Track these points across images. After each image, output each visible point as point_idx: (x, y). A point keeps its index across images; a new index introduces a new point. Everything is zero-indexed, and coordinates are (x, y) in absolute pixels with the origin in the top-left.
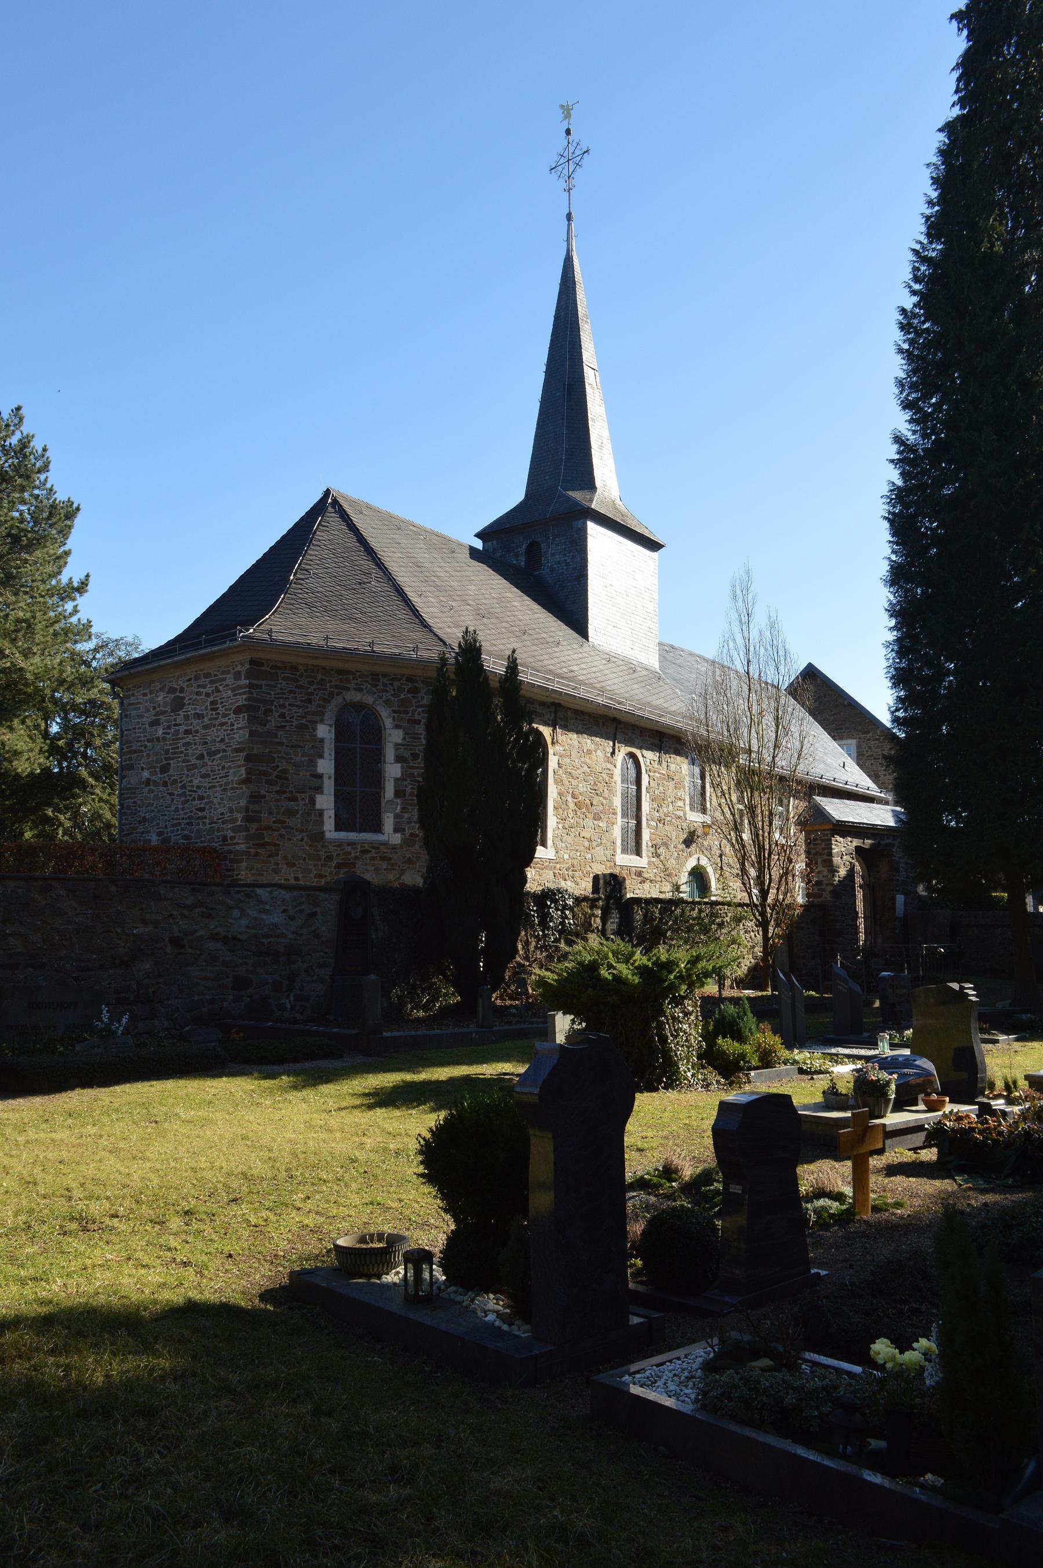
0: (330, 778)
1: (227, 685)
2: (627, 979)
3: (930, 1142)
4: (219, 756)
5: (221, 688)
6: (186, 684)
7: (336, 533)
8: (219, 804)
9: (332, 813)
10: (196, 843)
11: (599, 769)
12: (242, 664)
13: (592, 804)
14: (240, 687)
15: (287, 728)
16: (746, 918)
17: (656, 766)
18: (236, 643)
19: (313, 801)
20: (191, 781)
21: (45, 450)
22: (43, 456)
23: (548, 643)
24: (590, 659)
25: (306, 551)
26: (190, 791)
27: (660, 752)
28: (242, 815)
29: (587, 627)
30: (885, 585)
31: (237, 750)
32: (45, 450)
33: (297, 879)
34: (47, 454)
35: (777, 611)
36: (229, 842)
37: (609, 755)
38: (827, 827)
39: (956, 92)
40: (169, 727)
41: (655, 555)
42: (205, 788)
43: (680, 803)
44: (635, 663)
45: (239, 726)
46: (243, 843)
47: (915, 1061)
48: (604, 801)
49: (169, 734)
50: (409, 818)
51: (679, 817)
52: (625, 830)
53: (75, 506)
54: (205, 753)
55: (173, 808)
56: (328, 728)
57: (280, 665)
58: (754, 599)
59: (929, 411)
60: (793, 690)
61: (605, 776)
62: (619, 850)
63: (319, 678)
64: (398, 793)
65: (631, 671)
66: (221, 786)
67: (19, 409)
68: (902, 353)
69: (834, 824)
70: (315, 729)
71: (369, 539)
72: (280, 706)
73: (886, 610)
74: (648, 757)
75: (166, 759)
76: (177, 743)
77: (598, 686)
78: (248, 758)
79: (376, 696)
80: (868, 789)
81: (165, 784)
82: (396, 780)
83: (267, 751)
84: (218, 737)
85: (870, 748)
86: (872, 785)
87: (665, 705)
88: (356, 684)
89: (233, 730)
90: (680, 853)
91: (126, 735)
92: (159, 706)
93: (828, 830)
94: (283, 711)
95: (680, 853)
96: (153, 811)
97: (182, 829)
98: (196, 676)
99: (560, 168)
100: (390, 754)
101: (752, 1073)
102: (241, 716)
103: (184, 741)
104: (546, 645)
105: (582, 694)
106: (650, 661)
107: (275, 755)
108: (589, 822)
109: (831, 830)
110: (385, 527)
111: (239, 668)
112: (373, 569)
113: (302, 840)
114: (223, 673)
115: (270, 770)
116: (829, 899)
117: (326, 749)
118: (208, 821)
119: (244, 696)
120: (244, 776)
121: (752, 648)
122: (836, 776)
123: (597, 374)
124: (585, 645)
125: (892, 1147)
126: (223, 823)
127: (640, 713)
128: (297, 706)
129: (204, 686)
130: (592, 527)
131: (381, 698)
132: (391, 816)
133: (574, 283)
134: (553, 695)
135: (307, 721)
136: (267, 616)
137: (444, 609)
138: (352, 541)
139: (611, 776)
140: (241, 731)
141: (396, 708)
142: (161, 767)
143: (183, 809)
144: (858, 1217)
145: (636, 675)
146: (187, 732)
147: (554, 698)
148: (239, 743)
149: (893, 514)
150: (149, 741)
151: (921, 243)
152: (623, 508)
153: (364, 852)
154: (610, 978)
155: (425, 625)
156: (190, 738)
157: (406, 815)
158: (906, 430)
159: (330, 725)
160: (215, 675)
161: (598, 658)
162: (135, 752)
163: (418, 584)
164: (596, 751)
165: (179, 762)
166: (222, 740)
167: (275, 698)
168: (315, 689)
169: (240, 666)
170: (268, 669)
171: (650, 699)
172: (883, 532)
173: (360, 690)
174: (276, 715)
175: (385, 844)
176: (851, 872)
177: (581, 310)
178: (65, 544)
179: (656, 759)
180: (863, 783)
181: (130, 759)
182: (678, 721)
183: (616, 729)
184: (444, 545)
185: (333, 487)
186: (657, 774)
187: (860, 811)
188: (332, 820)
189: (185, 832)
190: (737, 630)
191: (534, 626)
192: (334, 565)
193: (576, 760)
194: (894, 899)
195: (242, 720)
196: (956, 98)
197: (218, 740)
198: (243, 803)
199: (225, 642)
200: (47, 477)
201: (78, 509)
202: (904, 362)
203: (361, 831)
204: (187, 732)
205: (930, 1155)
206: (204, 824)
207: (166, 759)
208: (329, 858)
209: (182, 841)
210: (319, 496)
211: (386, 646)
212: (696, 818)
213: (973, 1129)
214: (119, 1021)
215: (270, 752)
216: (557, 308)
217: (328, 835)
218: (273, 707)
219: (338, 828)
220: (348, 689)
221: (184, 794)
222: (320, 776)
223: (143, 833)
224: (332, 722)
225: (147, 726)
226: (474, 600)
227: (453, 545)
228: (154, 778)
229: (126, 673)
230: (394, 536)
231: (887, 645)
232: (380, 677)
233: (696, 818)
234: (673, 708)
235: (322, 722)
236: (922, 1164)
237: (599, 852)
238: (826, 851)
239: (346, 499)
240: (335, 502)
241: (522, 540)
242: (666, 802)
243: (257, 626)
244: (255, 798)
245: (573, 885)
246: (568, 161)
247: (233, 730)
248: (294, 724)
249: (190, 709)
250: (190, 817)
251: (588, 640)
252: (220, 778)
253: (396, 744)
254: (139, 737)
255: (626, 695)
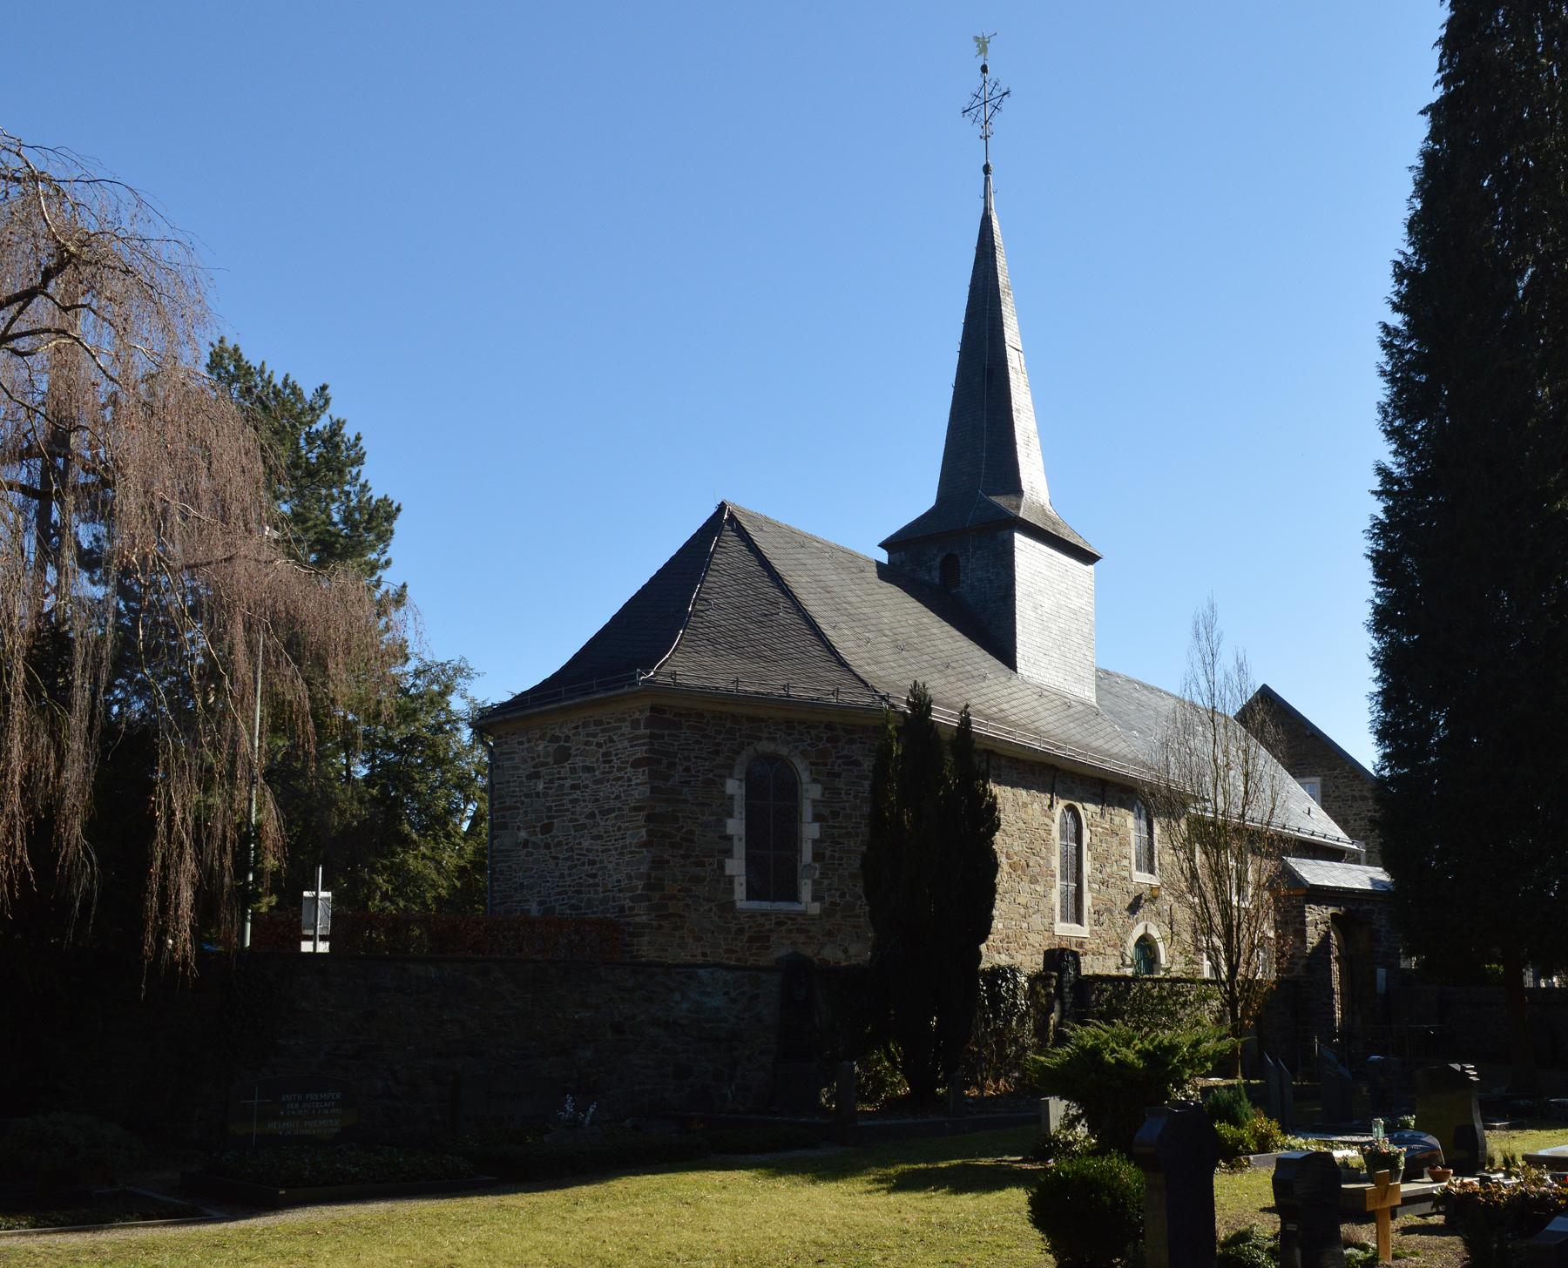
0: (740, 840)
1: (623, 735)
2: (1133, 1062)
3: (1437, 1208)
4: (613, 815)
5: (615, 738)
6: (572, 732)
7: (736, 555)
8: (615, 869)
9: (743, 879)
10: (587, 914)
11: (1035, 825)
12: (641, 712)
13: (1028, 866)
14: (637, 737)
15: (692, 784)
16: (1211, 997)
17: (1098, 819)
18: (636, 688)
19: (722, 866)
20: (580, 844)
21: (358, 438)
22: (356, 445)
23: (973, 677)
24: (1020, 694)
25: (704, 577)
26: (578, 854)
27: (1103, 805)
28: (642, 883)
29: (1014, 657)
30: (1369, 630)
31: (636, 809)
32: (358, 438)
33: (704, 955)
34: (362, 443)
35: (1245, 651)
36: (627, 913)
37: (1046, 808)
38: (1300, 892)
39: (1439, 71)
40: (551, 781)
41: (1091, 568)
42: (597, 850)
43: (1125, 862)
44: (1069, 696)
45: (638, 781)
46: (644, 915)
47: (1420, 1137)
48: (1042, 862)
49: (551, 788)
50: (830, 885)
51: (1125, 879)
52: (1064, 894)
53: (395, 505)
54: (596, 812)
55: (557, 873)
56: (737, 782)
57: (683, 712)
58: (1219, 638)
59: (1416, 438)
60: (1244, 716)
61: (1042, 832)
62: (1058, 918)
63: (727, 727)
64: (817, 856)
65: (1065, 707)
66: (616, 849)
67: (324, 388)
68: (1385, 375)
69: (1307, 888)
70: (723, 785)
71: (774, 562)
72: (685, 758)
73: (1370, 658)
74: (1088, 810)
75: (548, 817)
76: (562, 800)
77: (1031, 726)
78: (649, 818)
79: (791, 746)
80: (1338, 841)
81: (547, 846)
82: (815, 841)
83: (670, 809)
84: (613, 793)
85: (1337, 787)
86: (1341, 834)
87: (1106, 747)
88: (770, 733)
89: (631, 785)
90: (1126, 920)
91: (498, 789)
92: (539, 756)
93: (1301, 895)
94: (689, 764)
95: (1126, 920)
96: (532, 877)
97: (569, 898)
98: (584, 723)
99: (974, 111)
100: (807, 812)
101: (1251, 1157)
102: (641, 770)
103: (571, 797)
104: (972, 680)
105: (1019, 740)
106: (1086, 693)
107: (680, 815)
108: (1025, 885)
109: (1303, 895)
110: (788, 546)
111: (637, 715)
112: (781, 597)
113: (710, 910)
114: (619, 720)
115: (674, 832)
116: (1302, 974)
117: (736, 807)
118: (601, 890)
119: (644, 748)
120: (644, 839)
121: (1217, 693)
122: (1300, 825)
123: (1021, 355)
124: (1014, 677)
125: (1403, 1214)
126: (620, 891)
127: (1080, 759)
128: (702, 758)
129: (595, 736)
130: (1021, 542)
131: (797, 748)
132: (809, 882)
133: (994, 248)
134: (987, 742)
135: (715, 775)
136: (667, 656)
137: (861, 643)
138: (754, 566)
139: (1049, 832)
140: (640, 787)
141: (814, 760)
142: (542, 827)
143: (570, 875)
144: (1380, 1262)
145: (1071, 711)
146: (574, 787)
147: (986, 745)
148: (638, 801)
149: (1376, 551)
150: (526, 796)
151: (1404, 254)
152: (1053, 514)
153: (780, 923)
154: (1113, 1061)
155: (843, 664)
156: (577, 794)
157: (826, 882)
158: (1389, 461)
159: (741, 780)
160: (610, 723)
161: (1028, 692)
162: (509, 809)
163: (829, 614)
164: (1032, 804)
165: (564, 821)
166: (618, 797)
167: (679, 749)
168: (723, 739)
169: (638, 713)
170: (671, 717)
171: (1088, 740)
172: (1366, 570)
173: (773, 739)
174: (680, 768)
175: (803, 914)
176: (1326, 938)
177: (1002, 280)
178: (385, 552)
179: (1098, 811)
180: (1332, 833)
181: (503, 816)
182: (1124, 767)
183: (1054, 777)
184: (848, 561)
185: (727, 499)
186: (1099, 829)
187: (1336, 873)
188: (744, 887)
189: (573, 902)
190: (1200, 672)
191: (957, 658)
192: (736, 593)
193: (1011, 815)
194: (1374, 973)
195: (641, 776)
196: (1439, 76)
197: (613, 796)
198: (644, 869)
199: (623, 686)
200: (360, 471)
201: (398, 509)
202: (1387, 385)
203: (774, 900)
204: (574, 787)
205: (1438, 1219)
206: (596, 892)
207: (548, 817)
208: (740, 931)
209: (568, 911)
210: (712, 510)
211: (803, 690)
212: (1142, 878)
213: (1476, 1193)
214: (585, 1111)
215: (673, 811)
216: (973, 276)
217: (739, 905)
218: (677, 760)
219: (749, 898)
220: (760, 739)
221: (570, 858)
222: (730, 838)
223: (520, 901)
224: (743, 776)
225: (524, 779)
226: (890, 630)
227: (861, 563)
228: (533, 839)
229: (500, 718)
230: (797, 556)
231: (1373, 696)
232: (796, 724)
233: (1142, 878)
234: (1115, 750)
235: (731, 776)
236: (1431, 1226)
237: (1036, 920)
238: (1298, 920)
239: (743, 513)
240: (731, 515)
241: (935, 552)
242: (1109, 861)
243: (659, 668)
244: (658, 863)
245: (1008, 959)
246: (985, 103)
247: (631, 785)
248: (700, 778)
249: (579, 761)
250: (580, 885)
251: (1017, 673)
252: (616, 840)
253: (814, 801)
254: (514, 791)
255: (1063, 736)
